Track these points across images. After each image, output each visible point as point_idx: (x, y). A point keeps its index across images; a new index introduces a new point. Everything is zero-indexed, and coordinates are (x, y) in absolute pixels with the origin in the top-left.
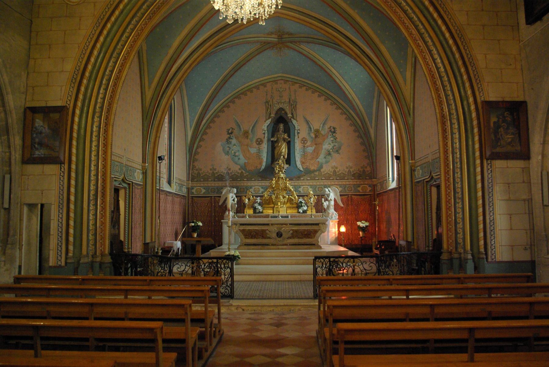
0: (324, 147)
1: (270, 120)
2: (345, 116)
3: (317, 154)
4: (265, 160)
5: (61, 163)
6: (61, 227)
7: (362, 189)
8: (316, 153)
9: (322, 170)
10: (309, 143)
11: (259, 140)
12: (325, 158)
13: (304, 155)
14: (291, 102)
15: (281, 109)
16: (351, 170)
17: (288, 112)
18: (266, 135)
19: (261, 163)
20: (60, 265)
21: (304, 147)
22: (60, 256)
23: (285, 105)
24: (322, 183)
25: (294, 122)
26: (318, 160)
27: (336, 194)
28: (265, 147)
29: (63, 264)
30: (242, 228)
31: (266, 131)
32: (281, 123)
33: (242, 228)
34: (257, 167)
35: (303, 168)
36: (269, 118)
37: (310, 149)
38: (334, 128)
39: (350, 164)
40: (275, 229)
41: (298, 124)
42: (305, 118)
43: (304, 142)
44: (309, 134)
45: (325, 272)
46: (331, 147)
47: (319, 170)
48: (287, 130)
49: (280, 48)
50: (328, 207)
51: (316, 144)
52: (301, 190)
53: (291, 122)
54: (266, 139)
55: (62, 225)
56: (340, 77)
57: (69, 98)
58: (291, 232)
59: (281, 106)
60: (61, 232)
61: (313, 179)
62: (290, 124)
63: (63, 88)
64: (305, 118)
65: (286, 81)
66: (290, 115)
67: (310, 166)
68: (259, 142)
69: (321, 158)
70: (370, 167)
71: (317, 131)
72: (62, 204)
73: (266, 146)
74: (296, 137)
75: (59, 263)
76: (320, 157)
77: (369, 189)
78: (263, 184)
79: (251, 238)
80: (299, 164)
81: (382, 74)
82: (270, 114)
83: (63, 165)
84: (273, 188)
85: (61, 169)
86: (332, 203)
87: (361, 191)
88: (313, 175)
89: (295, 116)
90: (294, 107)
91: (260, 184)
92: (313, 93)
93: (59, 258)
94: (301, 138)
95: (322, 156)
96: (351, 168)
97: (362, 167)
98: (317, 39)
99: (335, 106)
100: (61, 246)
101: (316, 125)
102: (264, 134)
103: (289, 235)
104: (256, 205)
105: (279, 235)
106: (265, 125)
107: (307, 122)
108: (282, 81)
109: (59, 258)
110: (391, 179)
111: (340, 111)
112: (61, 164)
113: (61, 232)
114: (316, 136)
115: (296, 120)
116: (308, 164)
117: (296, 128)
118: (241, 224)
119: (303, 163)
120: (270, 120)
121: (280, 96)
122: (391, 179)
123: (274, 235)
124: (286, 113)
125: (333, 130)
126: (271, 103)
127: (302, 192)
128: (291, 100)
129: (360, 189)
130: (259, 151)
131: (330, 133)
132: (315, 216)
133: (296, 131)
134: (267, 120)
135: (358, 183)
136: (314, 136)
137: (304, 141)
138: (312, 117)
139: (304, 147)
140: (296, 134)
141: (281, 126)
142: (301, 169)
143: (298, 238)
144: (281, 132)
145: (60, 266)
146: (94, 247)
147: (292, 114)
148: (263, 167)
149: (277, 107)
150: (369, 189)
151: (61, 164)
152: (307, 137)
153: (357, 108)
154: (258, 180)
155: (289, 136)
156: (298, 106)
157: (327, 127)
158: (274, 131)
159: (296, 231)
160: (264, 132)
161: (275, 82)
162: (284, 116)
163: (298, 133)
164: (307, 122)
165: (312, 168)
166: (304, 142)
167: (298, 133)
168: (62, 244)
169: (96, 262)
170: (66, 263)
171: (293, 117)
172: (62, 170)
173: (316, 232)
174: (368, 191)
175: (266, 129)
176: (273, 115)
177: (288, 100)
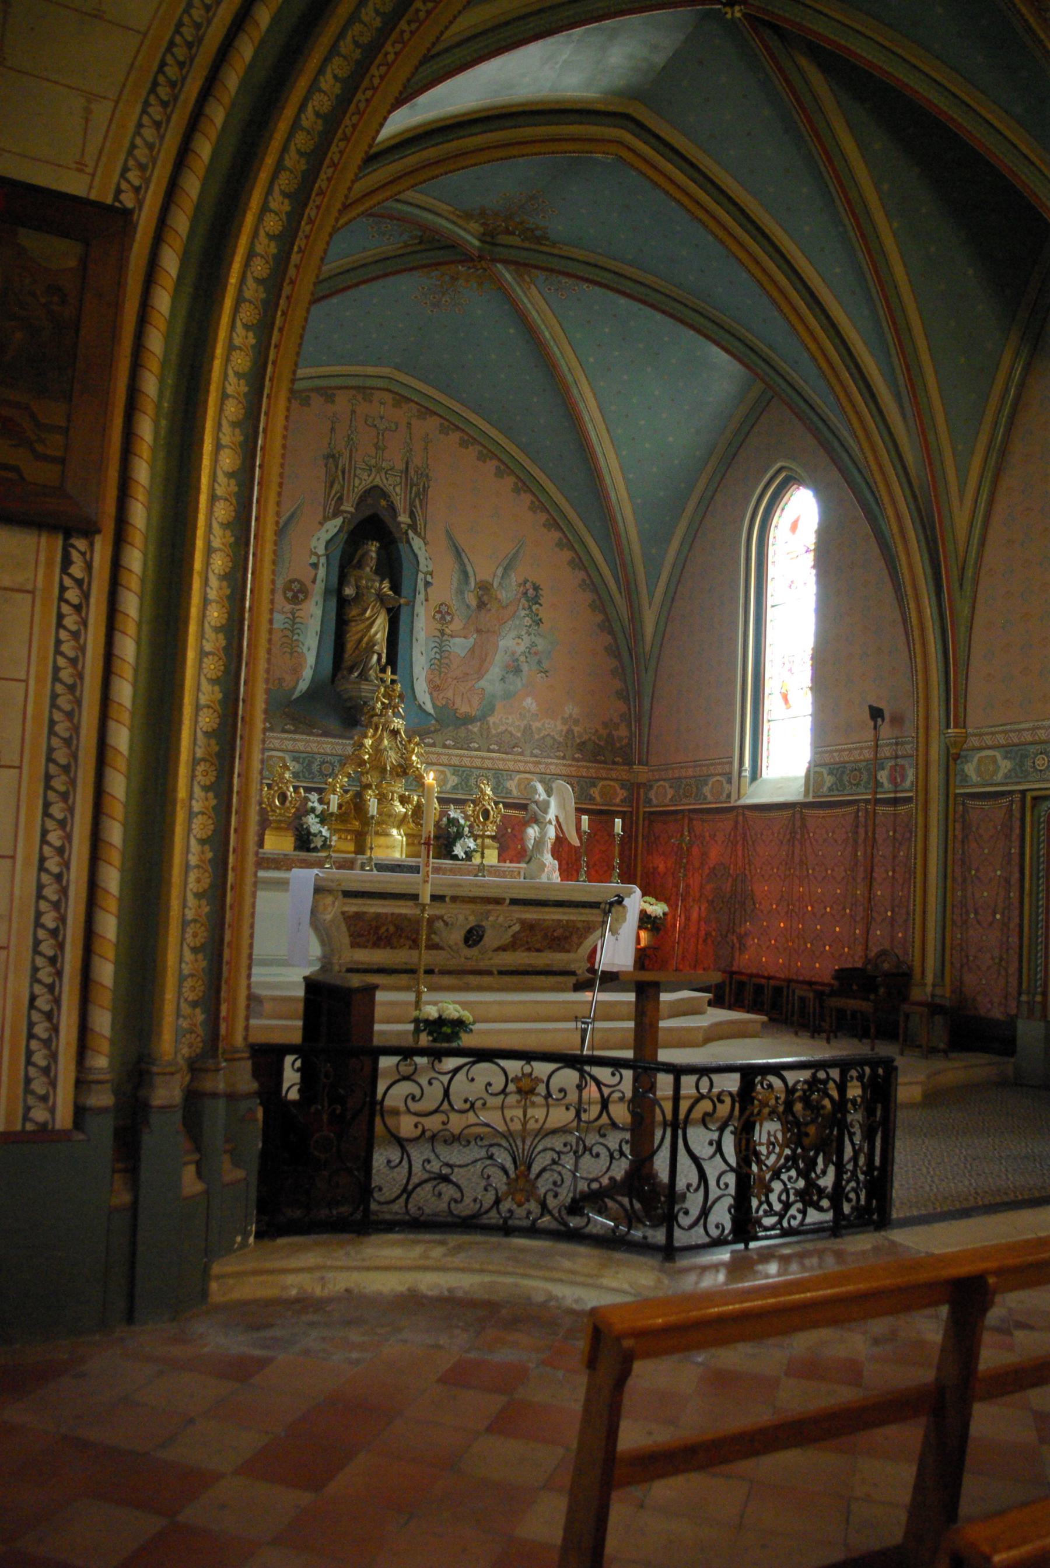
0: (502, 643)
1: (338, 521)
2: (567, 555)
3: (483, 661)
4: (311, 659)
5: (71, 527)
6: (56, 906)
7: (603, 794)
8: (479, 658)
9: (491, 720)
10: (457, 625)
11: (296, 586)
12: (503, 679)
13: (440, 662)
14: (412, 473)
15: (375, 492)
16: (576, 729)
17: (400, 505)
18: (322, 572)
19: (296, 671)
20: (43, 1127)
21: (442, 633)
22: (46, 1071)
23: (391, 480)
24: (488, 763)
25: (417, 543)
26: (482, 683)
27: (562, 805)
28: (314, 613)
29: (64, 1118)
30: (353, 907)
31: (323, 560)
32: (374, 542)
33: (353, 907)
34: (281, 680)
35: (435, 706)
36: (335, 515)
37: (459, 646)
38: (536, 588)
39: (570, 709)
40: (464, 918)
41: (426, 553)
42: (451, 538)
43: (443, 618)
44: (460, 592)
45: (854, 1091)
46: (522, 648)
47: (483, 718)
48: (392, 567)
49: (454, 278)
50: (539, 843)
51: (479, 631)
52: (512, 785)
53: (408, 542)
54: (319, 588)
55: (64, 891)
56: (602, 427)
57: (134, 176)
58: (517, 928)
59: (377, 481)
60: (54, 933)
61: (463, 744)
62: (402, 547)
63: (101, 112)
64: (451, 538)
65: (401, 400)
66: (404, 518)
67: (458, 702)
68: (297, 593)
69: (491, 681)
70: (629, 725)
71: (484, 588)
72: (66, 769)
73: (318, 612)
74: (420, 597)
75: (39, 1114)
76: (488, 677)
77: (622, 794)
78: (300, 746)
79: (375, 945)
80: (421, 687)
81: (843, 445)
82: (340, 500)
83: (81, 544)
84: (363, 763)
85: (67, 562)
86: (551, 832)
87: (598, 798)
88: (462, 732)
89: (420, 522)
90: (418, 494)
91: (289, 745)
92: (481, 458)
93: (39, 1086)
94: (434, 602)
95: (495, 671)
96: (576, 722)
97: (605, 725)
98: (636, 282)
99: (543, 517)
100: (49, 1016)
101: (483, 569)
102: (315, 566)
103: (507, 938)
104: (312, 823)
105: (473, 937)
106: (321, 536)
107: (458, 553)
108: (387, 397)
109: (39, 1086)
110: (747, 774)
111: (558, 535)
112: (68, 535)
113: (54, 933)
114: (481, 605)
115: (424, 539)
116: (449, 694)
117: (422, 567)
118: (348, 894)
119: (435, 688)
120: (338, 521)
121: (376, 446)
122: (747, 774)
123: (457, 936)
124: (392, 509)
125: (531, 592)
126: (344, 461)
127: (515, 793)
128: (411, 466)
129: (595, 792)
130: (294, 623)
131: (523, 600)
132: (493, 871)
133: (421, 576)
134: (326, 519)
135: (592, 773)
136: (474, 603)
137: (443, 614)
138: (473, 541)
139: (442, 633)
140: (421, 585)
141: (373, 548)
142: (429, 707)
143: (529, 950)
144: (368, 569)
145: (44, 1133)
146: (200, 1016)
147: (412, 515)
148: (303, 686)
149: (364, 481)
150: (622, 794)
151: (68, 535)
152: (455, 604)
153: (623, 535)
154: (284, 731)
155: (396, 588)
156: (430, 493)
157: (514, 579)
158: (346, 559)
159: (529, 927)
160: (314, 559)
161: (365, 391)
162: (386, 517)
163: (427, 584)
164: (458, 553)
165: (464, 709)
166: (443, 618)
167: (427, 584)
168: (57, 1001)
169: (215, 1095)
170: (80, 1112)
171: (413, 527)
172: (77, 570)
173: (589, 928)
174: (618, 800)
175: (321, 551)
176: (348, 507)
177: (400, 466)
